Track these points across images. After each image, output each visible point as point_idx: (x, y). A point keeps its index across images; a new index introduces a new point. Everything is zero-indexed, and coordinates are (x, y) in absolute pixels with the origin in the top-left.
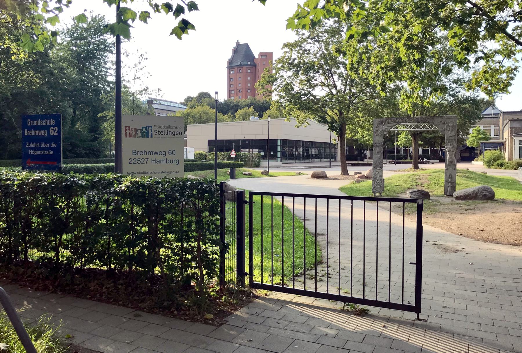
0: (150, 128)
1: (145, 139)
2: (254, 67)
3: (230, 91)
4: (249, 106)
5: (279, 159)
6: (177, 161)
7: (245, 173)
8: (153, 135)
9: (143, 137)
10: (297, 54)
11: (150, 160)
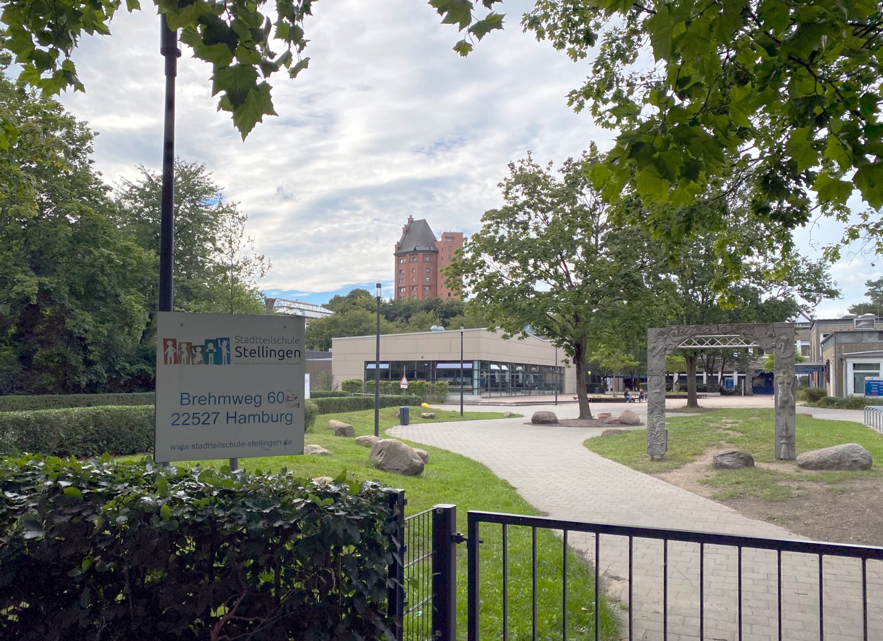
0: (225, 342)
1: (212, 367)
2: (435, 254)
3: (398, 289)
4: (428, 309)
5: (476, 392)
6: (289, 417)
7: (425, 414)
8: (232, 357)
9: (207, 363)
10: (507, 229)
11: (222, 418)
